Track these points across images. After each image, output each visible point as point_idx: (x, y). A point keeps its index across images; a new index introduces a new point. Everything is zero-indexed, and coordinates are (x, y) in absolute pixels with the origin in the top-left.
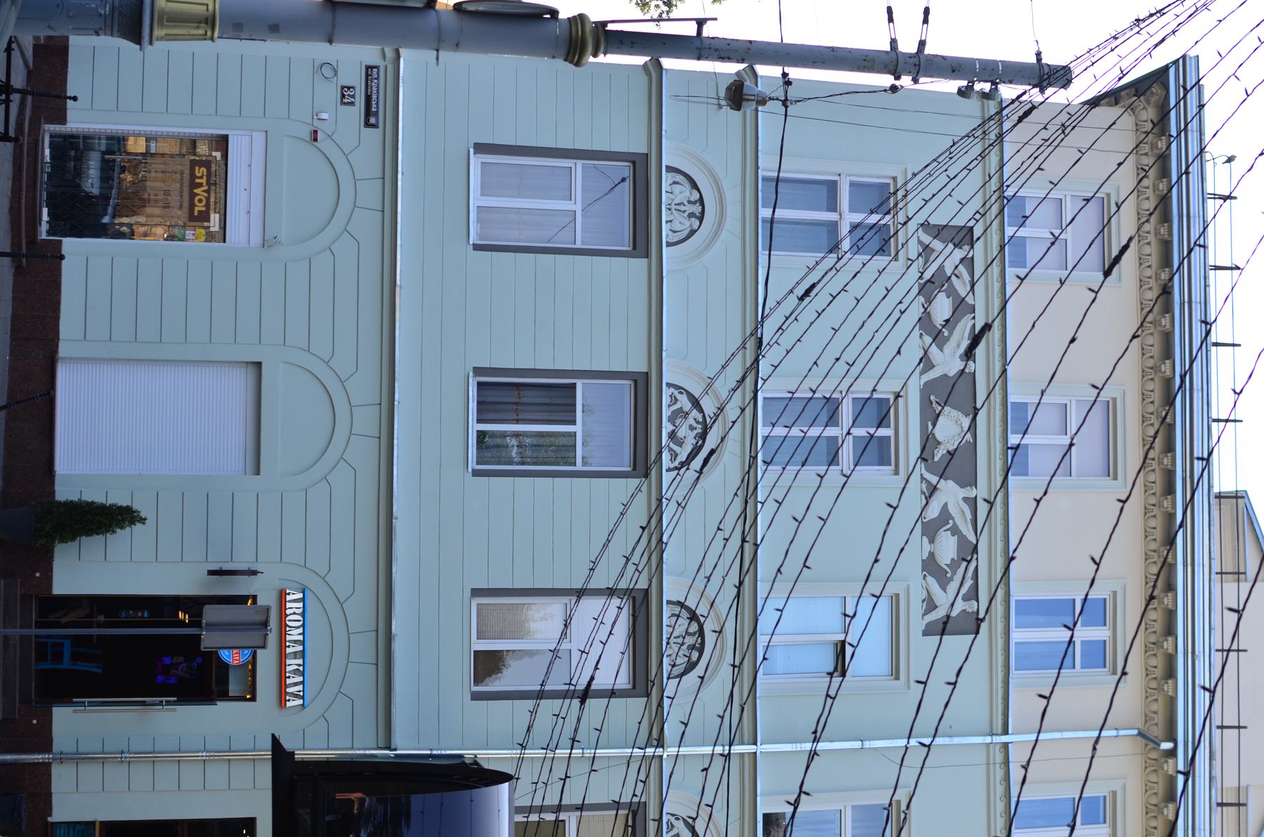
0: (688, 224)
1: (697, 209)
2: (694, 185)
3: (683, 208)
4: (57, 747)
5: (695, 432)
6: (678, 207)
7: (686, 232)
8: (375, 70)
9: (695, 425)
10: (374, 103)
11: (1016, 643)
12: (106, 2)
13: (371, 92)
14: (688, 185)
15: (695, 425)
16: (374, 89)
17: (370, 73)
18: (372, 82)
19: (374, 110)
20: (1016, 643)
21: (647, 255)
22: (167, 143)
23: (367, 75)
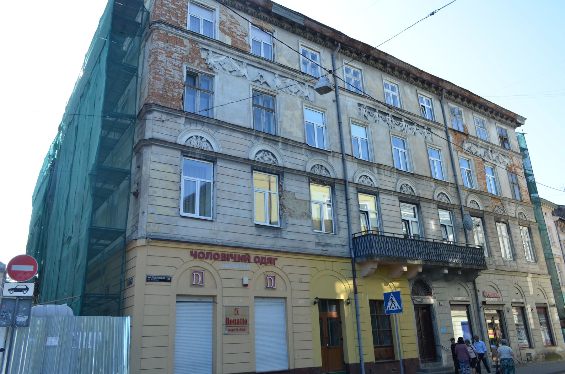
0: (205, 143)
1: (199, 138)
2: (192, 137)
3: (199, 143)
4: (358, 362)
5: (267, 155)
6: (199, 144)
7: (207, 143)
8: (148, 278)
9: (265, 154)
10: (162, 278)
11: (200, 215)
12: (97, 370)
13: (157, 279)
14: (191, 139)
15: (265, 154)
16: (156, 278)
17: (149, 280)
18: (153, 279)
19: (164, 278)
20: (200, 215)
21: (216, 158)
22: (519, 321)
23: (150, 281)
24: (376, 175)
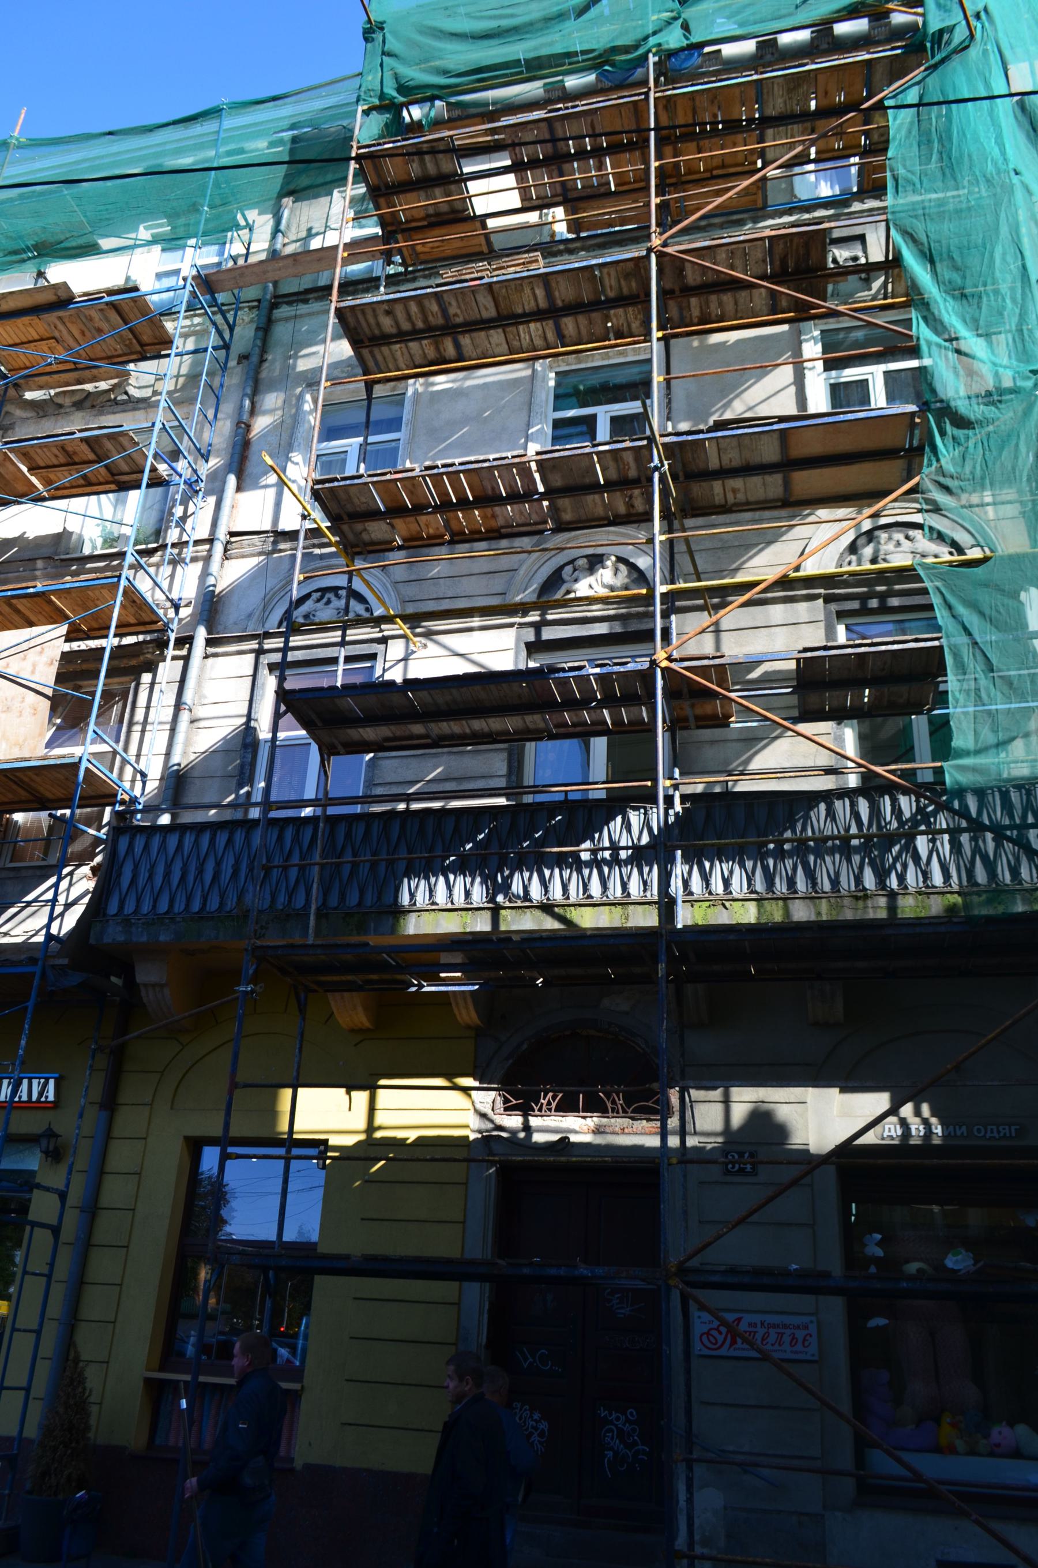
9: (325, 600)
24: (400, 573)
